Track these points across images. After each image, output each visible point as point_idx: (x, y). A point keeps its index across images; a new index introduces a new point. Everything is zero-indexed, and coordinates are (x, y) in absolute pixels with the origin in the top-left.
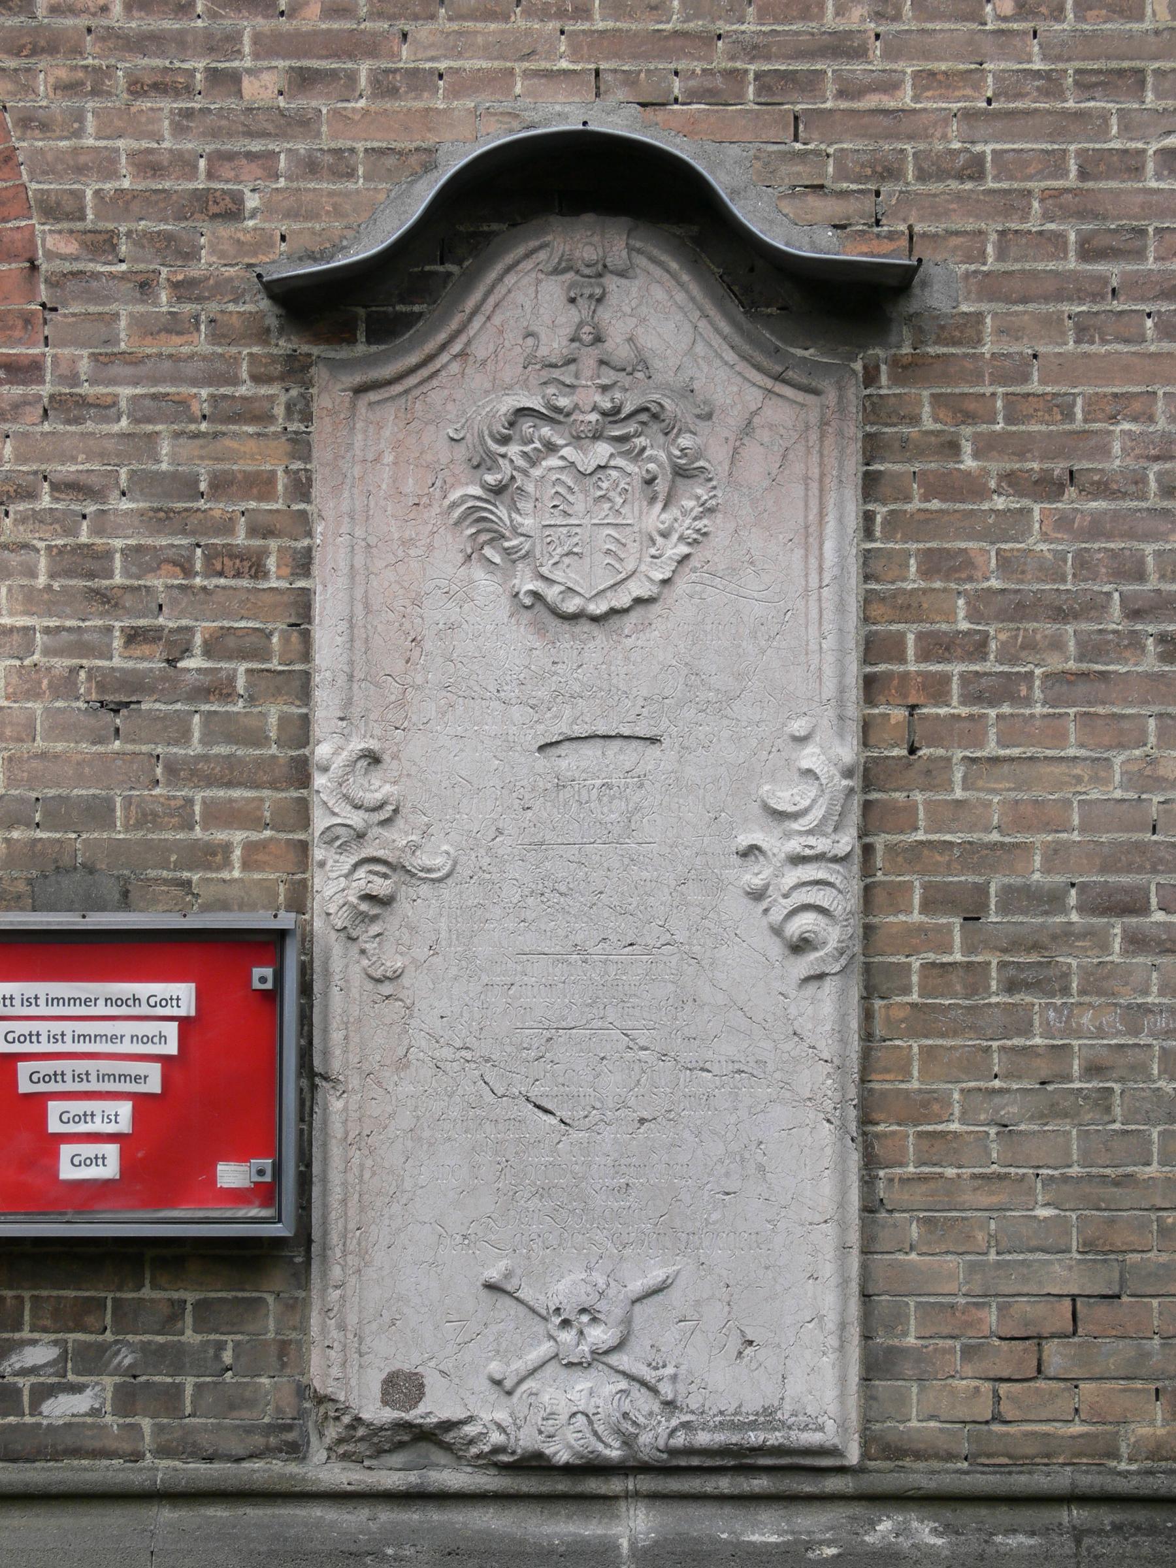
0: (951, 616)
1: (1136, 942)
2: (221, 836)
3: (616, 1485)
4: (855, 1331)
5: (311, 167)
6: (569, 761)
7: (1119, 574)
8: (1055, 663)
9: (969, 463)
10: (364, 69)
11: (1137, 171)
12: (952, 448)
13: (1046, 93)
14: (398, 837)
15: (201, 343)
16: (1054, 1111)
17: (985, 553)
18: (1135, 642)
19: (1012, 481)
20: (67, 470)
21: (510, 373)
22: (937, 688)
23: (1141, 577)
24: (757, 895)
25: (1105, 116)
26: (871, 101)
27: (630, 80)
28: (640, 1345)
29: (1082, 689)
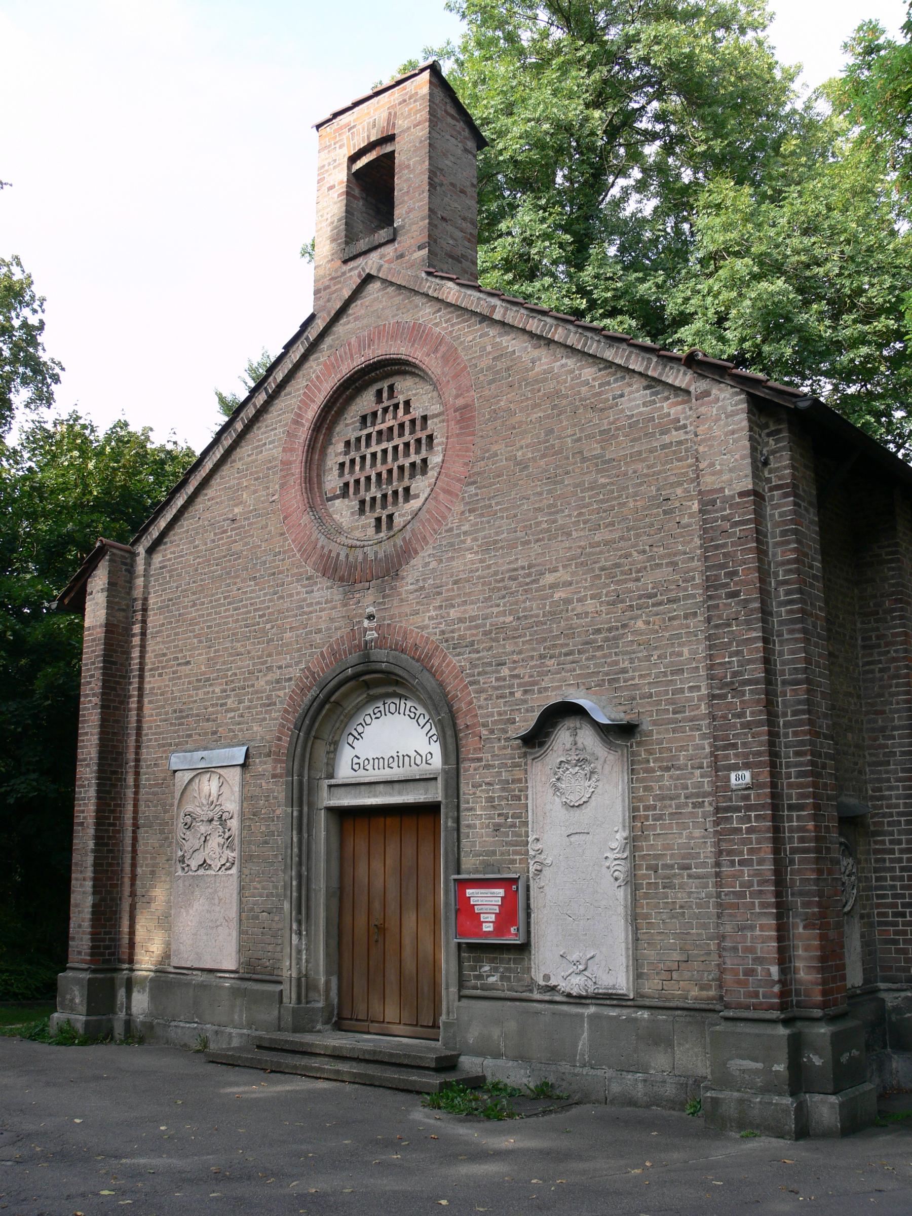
0: (649, 801)
1: (689, 876)
2: (515, 857)
3: (588, 1001)
4: (631, 968)
5: (527, 711)
6: (573, 838)
7: (683, 789)
8: (671, 810)
9: (652, 765)
10: (536, 688)
11: (683, 692)
12: (648, 761)
13: (664, 676)
14: (542, 856)
15: (509, 751)
16: (672, 917)
17: (655, 786)
18: (687, 804)
19: (661, 768)
20: (487, 780)
21: (560, 753)
22: (647, 818)
23: (687, 789)
24: (608, 868)
25: (676, 680)
26: (630, 683)
27: (584, 684)
28: (589, 970)
29: (676, 816)
